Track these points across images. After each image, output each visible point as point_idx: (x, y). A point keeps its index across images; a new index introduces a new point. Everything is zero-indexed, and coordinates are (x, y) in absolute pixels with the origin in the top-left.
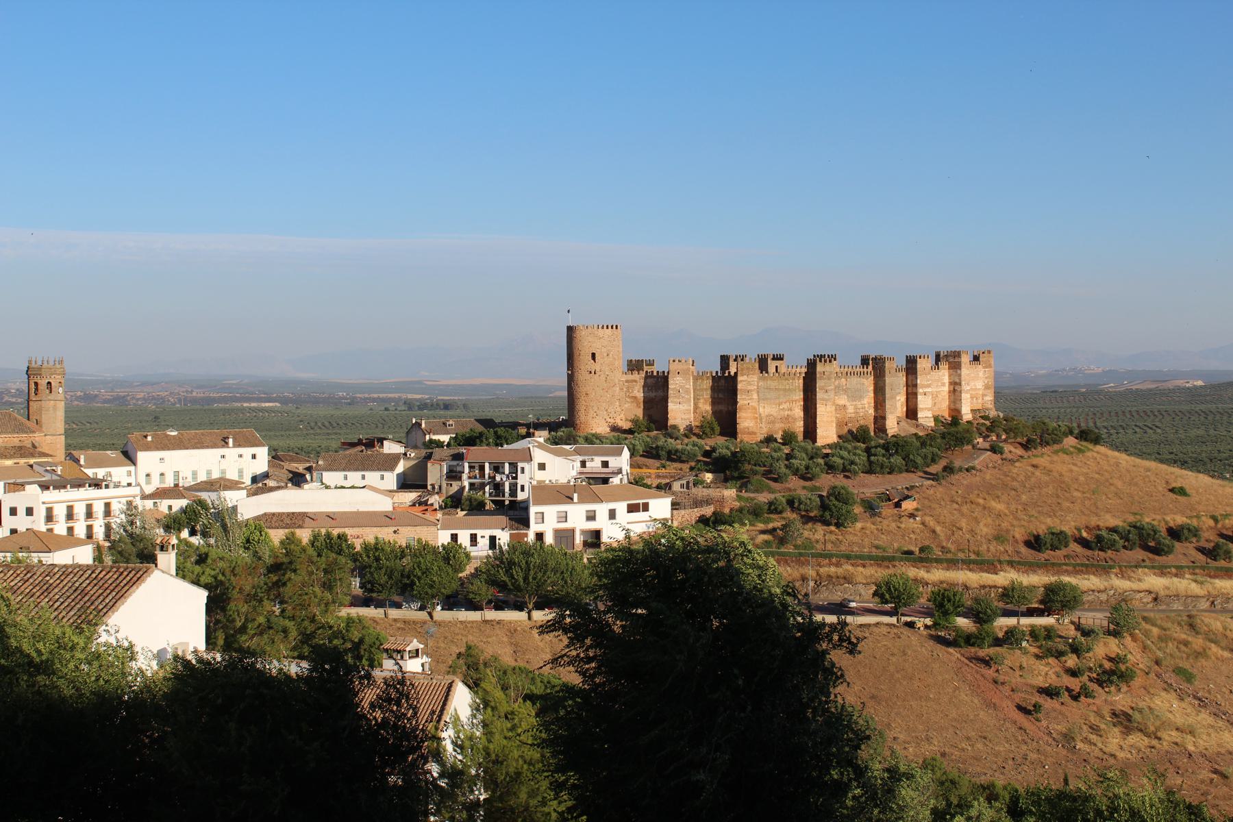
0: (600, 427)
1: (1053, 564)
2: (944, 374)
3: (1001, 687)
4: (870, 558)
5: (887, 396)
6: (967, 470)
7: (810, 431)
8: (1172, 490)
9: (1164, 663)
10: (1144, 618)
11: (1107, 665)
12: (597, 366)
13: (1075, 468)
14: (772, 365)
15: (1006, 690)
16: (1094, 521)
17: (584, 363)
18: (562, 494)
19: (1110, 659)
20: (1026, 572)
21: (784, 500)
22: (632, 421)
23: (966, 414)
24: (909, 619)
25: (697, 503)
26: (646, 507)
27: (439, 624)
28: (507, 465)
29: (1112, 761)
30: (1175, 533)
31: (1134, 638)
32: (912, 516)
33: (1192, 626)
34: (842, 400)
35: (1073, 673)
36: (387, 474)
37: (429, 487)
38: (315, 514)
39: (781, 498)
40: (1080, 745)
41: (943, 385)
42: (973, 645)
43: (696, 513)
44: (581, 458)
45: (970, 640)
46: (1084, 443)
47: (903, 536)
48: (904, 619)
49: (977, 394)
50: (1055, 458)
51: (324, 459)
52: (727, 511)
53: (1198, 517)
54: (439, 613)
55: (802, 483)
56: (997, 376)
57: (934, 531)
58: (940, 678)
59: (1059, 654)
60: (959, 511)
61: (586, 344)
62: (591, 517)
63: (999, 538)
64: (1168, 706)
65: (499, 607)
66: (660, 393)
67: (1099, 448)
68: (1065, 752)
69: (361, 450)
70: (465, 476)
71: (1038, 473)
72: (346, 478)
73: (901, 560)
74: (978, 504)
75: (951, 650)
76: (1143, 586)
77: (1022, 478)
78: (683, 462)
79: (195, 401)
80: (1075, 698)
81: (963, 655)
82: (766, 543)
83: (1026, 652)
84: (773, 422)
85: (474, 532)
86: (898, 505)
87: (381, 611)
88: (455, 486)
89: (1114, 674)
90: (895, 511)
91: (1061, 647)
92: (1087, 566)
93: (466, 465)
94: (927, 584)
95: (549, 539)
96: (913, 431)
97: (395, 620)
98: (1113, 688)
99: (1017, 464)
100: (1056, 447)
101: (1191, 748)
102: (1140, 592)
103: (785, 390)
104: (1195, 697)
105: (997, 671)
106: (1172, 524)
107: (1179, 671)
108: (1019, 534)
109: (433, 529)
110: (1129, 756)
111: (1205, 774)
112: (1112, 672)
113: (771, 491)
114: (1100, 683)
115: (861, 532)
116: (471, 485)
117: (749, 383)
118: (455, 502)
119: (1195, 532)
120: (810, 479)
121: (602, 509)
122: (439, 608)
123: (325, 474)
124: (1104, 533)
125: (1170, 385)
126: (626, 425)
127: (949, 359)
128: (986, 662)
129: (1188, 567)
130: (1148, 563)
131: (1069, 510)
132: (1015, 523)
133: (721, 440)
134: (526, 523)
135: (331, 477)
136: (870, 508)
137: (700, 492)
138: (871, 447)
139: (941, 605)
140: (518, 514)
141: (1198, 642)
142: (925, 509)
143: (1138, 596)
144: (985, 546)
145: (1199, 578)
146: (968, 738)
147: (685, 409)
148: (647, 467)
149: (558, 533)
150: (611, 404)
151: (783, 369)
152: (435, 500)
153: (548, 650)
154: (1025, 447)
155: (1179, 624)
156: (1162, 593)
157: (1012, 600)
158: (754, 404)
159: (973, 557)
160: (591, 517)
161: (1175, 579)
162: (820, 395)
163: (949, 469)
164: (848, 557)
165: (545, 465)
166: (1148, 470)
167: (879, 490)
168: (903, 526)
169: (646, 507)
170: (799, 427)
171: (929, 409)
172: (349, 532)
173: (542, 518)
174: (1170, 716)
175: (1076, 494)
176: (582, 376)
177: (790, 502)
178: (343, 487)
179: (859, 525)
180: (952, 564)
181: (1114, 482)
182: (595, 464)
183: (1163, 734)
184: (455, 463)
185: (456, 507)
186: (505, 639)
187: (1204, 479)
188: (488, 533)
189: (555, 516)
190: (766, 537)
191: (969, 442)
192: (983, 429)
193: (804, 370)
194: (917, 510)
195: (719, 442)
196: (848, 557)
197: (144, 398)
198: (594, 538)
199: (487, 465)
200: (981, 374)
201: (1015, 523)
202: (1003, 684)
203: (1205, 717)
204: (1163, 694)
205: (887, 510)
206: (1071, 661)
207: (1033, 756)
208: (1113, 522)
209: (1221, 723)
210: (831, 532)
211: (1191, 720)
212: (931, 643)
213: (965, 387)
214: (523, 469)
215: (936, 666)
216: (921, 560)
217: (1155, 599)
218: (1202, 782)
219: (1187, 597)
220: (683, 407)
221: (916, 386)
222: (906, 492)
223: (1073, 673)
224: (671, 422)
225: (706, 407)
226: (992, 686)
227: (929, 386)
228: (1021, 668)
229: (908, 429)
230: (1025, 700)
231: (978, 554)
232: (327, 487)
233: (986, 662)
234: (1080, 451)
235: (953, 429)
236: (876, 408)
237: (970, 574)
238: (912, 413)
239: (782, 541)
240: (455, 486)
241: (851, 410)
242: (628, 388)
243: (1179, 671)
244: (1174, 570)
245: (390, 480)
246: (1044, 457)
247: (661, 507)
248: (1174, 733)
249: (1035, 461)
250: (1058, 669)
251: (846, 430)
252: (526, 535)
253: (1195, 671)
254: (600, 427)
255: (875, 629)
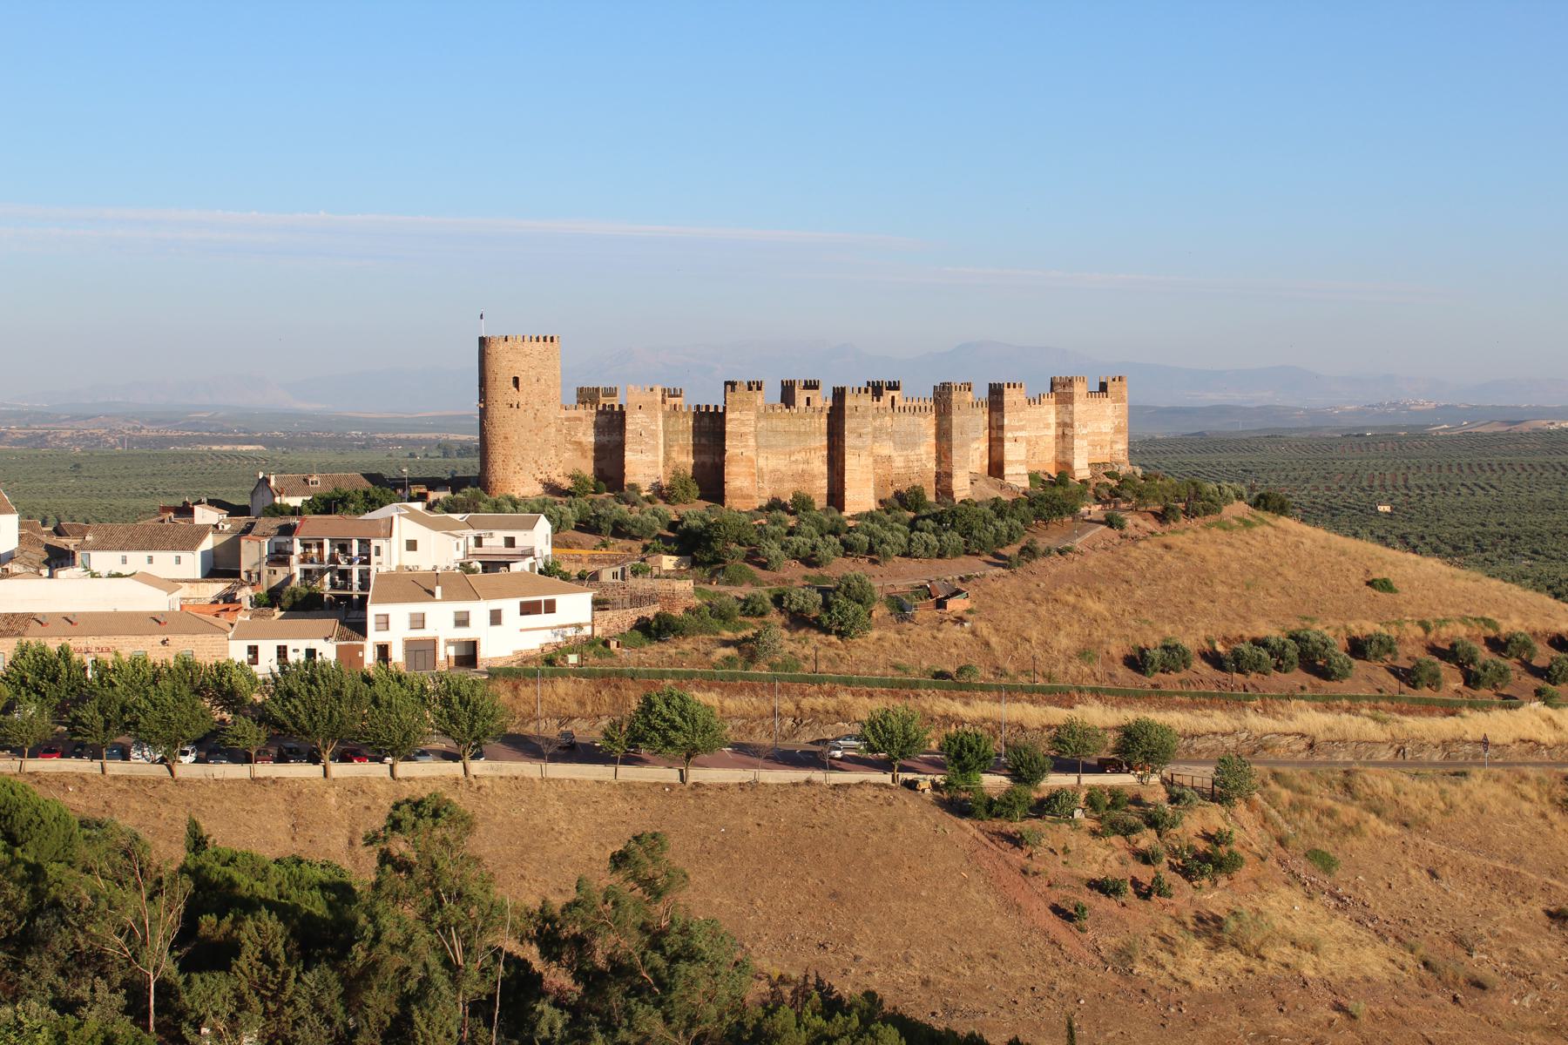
0: (526, 487)
1: (1162, 694)
2: (1049, 412)
3: (1032, 881)
4: (882, 683)
5: (955, 443)
6: (1061, 552)
7: (836, 496)
8: (1368, 583)
9: (1291, 842)
10: (1275, 776)
11: (1202, 846)
12: (521, 397)
13: (1227, 550)
14: (801, 396)
15: (1040, 885)
16: (1238, 629)
17: (502, 391)
18: (421, 587)
19: (1208, 837)
20: (1118, 705)
21: (767, 597)
22: (572, 477)
23: (1081, 469)
24: (910, 776)
25: (637, 600)
26: (550, 607)
27: (179, 783)
28: (355, 543)
29: (1185, 992)
30: (1358, 648)
31: (1251, 805)
32: (960, 620)
33: (1347, 788)
34: (886, 448)
35: (1146, 858)
36: (185, 556)
37: (244, 576)
38: (44, 615)
39: (764, 593)
40: (1140, 968)
41: (1047, 426)
42: (998, 815)
43: (632, 615)
44: (476, 533)
45: (992, 808)
46: (1260, 514)
47: (940, 651)
48: (904, 776)
49: (1100, 438)
50: (1204, 535)
51: (95, 533)
52: (678, 612)
53: (1399, 624)
54: (187, 765)
55: (805, 571)
56: (1136, 414)
57: (987, 644)
58: (942, 867)
59: (1128, 830)
60: (1034, 613)
61: (505, 364)
62: (462, 621)
63: (1084, 654)
64: (1286, 909)
65: (282, 759)
66: (618, 438)
67: (1284, 522)
68: (1115, 978)
69: (167, 524)
70: (294, 559)
71: (1168, 557)
72: (124, 561)
73: (929, 686)
74: (1067, 604)
75: (966, 823)
76: (1294, 726)
77: (1143, 564)
78: (633, 538)
79: (143, 442)
80: (1145, 895)
81: (982, 831)
82: (729, 661)
83: (1076, 826)
84: (781, 480)
85: (282, 643)
86: (941, 604)
87: (97, 763)
88: (281, 574)
89: (1211, 860)
90: (937, 613)
91: (1133, 820)
92: (1212, 696)
93: (297, 542)
94: (963, 722)
95: (397, 655)
96: (995, 493)
97: (115, 778)
98: (1205, 882)
99: (1141, 544)
100: (1210, 519)
101: (1308, 972)
102: (1286, 735)
103: (799, 433)
104: (1332, 895)
105: (1030, 855)
106: (1357, 633)
107: (1314, 855)
108: (1117, 648)
109: (221, 638)
110: (1213, 985)
111: (1324, 1012)
112: (1205, 858)
113: (755, 582)
114: (1186, 873)
115: (878, 644)
116: (307, 572)
117: (743, 423)
118: (273, 598)
119: (1387, 645)
120: (816, 565)
121: (479, 611)
122: (191, 758)
123: (94, 555)
124: (1244, 648)
125: (1525, 428)
126: (567, 484)
127: (811, 386)
128: (1016, 841)
129: (1368, 698)
130: (1307, 693)
131: (1205, 613)
132: (1115, 631)
133: (701, 506)
134: (361, 629)
135: (103, 561)
136: (900, 608)
137: (641, 584)
138: (922, 515)
139: (959, 756)
140: (350, 614)
141: (1349, 812)
142: (990, 612)
143: (1285, 741)
144: (1061, 667)
145: (1382, 715)
146: (970, 957)
147: (651, 459)
148: (580, 546)
149: (412, 647)
150: (542, 450)
151: (900, 402)
152: (245, 594)
153: (346, 823)
154: (1162, 517)
155: (1329, 784)
156: (1321, 737)
157: (1069, 752)
158: (750, 453)
159: (1041, 682)
160: (462, 621)
161: (1345, 716)
162: (850, 440)
163: (1029, 552)
164: (847, 682)
165: (414, 541)
166: (1344, 553)
167: (917, 583)
168: (940, 635)
169: (550, 607)
170: (819, 488)
171: (1021, 462)
172: (75, 643)
173: (384, 623)
174: (1288, 924)
175: (1220, 588)
176: (498, 411)
177: (778, 600)
178: (119, 575)
179: (874, 634)
180: (1012, 692)
181: (1303, 569)
182: (495, 542)
183: (1271, 953)
184: (283, 539)
185: (273, 606)
186: (282, 807)
187: (1432, 565)
188: (303, 645)
189: (407, 619)
190: (730, 651)
191: (1073, 511)
192: (1105, 492)
193: (829, 403)
194: (970, 611)
195: (694, 510)
196: (847, 682)
197: (71, 438)
198: (468, 655)
199: (327, 543)
200: (1109, 411)
201: (1115, 631)
202: (1036, 874)
203: (1342, 925)
204: (1284, 890)
205: (924, 612)
206: (1146, 839)
207: (1064, 985)
208: (1264, 629)
209: (1363, 934)
210: (830, 645)
211: (1318, 930)
212: (938, 812)
213: (1079, 430)
214: (378, 548)
215: (938, 847)
216: (960, 687)
217: (1311, 746)
218: (1317, 1024)
219: (1359, 742)
220: (648, 457)
221: (1001, 428)
222: (958, 585)
223: (1146, 858)
224: (628, 480)
225: (686, 461)
226: (1018, 878)
227: (1022, 428)
228: (1066, 851)
229: (988, 490)
230: (1066, 899)
231: (1049, 678)
232: (93, 575)
233: (1016, 841)
234: (1247, 524)
235: (1059, 491)
236: (939, 461)
237: (1030, 708)
238: (996, 468)
239: (752, 658)
240: (281, 574)
241: (899, 462)
242: (569, 429)
243: (1314, 855)
244: (1345, 703)
245: (192, 563)
246: (1187, 535)
247: (575, 608)
248: (1288, 950)
249: (1169, 539)
250: (1125, 853)
251: (891, 492)
252: (361, 648)
253: (1340, 856)
254: (526, 487)
255: (857, 793)
